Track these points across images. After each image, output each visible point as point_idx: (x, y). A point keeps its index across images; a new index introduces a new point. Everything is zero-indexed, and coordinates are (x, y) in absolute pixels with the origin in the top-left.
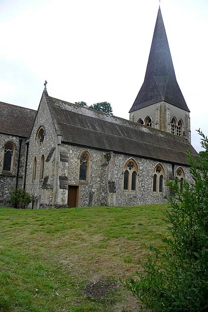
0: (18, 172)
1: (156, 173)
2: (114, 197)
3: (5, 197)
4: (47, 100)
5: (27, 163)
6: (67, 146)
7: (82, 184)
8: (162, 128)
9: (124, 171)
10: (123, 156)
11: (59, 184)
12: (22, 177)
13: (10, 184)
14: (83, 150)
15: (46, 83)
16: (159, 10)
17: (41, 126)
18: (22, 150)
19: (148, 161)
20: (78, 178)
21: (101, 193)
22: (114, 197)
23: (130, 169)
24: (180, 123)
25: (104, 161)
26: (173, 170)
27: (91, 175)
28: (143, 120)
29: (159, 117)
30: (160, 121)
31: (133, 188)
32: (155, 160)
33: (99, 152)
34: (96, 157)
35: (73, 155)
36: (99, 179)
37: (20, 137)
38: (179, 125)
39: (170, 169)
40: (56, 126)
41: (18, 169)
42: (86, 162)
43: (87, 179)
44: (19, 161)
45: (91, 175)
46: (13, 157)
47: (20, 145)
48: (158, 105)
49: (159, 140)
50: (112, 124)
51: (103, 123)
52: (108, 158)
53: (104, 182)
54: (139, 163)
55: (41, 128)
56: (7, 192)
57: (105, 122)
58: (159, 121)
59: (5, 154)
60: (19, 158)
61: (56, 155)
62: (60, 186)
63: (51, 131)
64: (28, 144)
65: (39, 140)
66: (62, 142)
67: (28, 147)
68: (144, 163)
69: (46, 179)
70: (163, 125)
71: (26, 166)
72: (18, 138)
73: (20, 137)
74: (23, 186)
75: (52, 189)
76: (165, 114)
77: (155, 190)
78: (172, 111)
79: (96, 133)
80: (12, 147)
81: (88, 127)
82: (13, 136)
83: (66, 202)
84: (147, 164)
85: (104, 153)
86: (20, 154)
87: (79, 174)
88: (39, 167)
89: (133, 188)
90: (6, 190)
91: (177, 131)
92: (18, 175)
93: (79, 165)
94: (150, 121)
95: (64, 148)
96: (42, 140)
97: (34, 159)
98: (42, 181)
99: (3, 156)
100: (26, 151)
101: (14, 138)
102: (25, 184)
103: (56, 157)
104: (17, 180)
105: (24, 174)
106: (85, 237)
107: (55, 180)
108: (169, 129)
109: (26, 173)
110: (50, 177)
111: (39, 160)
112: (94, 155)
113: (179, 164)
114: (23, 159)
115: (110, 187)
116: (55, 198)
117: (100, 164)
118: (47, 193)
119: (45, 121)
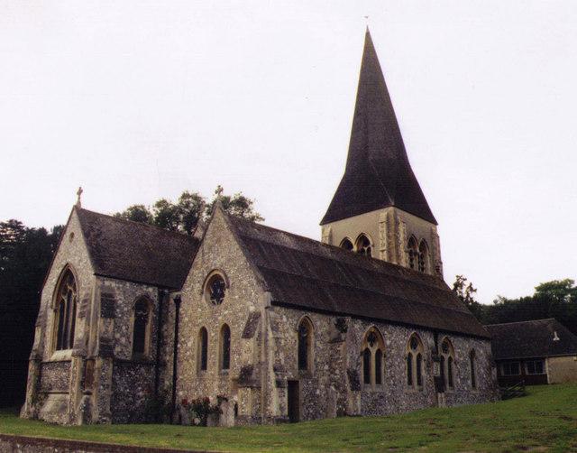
1: (411, 351)
2: (358, 397)
4: (81, 214)
8: (394, 258)
9: (364, 349)
10: (360, 322)
13: (145, 379)
14: (303, 315)
15: (80, 192)
16: (368, 34)
19: (398, 329)
20: (296, 366)
22: (358, 397)
23: (372, 346)
24: (423, 245)
25: (335, 332)
26: (436, 343)
27: (315, 360)
31: (378, 381)
32: (408, 326)
33: (326, 318)
34: (322, 325)
38: (421, 251)
39: (431, 341)
46: (148, 326)
53: (337, 372)
55: (215, 273)
56: (141, 393)
59: (136, 321)
64: (178, 301)
65: (209, 296)
70: (394, 252)
75: (259, 388)
76: (396, 230)
77: (410, 382)
78: (409, 221)
80: (147, 305)
82: (149, 285)
83: (286, 412)
84: (397, 336)
85: (334, 320)
87: (297, 359)
89: (378, 381)
97: (197, 329)
99: (133, 324)
101: (150, 289)
111: (214, 335)
112: (318, 323)
113: (445, 332)
114: (169, 329)
115: (113, 309)
116: (266, 405)
117: (328, 338)
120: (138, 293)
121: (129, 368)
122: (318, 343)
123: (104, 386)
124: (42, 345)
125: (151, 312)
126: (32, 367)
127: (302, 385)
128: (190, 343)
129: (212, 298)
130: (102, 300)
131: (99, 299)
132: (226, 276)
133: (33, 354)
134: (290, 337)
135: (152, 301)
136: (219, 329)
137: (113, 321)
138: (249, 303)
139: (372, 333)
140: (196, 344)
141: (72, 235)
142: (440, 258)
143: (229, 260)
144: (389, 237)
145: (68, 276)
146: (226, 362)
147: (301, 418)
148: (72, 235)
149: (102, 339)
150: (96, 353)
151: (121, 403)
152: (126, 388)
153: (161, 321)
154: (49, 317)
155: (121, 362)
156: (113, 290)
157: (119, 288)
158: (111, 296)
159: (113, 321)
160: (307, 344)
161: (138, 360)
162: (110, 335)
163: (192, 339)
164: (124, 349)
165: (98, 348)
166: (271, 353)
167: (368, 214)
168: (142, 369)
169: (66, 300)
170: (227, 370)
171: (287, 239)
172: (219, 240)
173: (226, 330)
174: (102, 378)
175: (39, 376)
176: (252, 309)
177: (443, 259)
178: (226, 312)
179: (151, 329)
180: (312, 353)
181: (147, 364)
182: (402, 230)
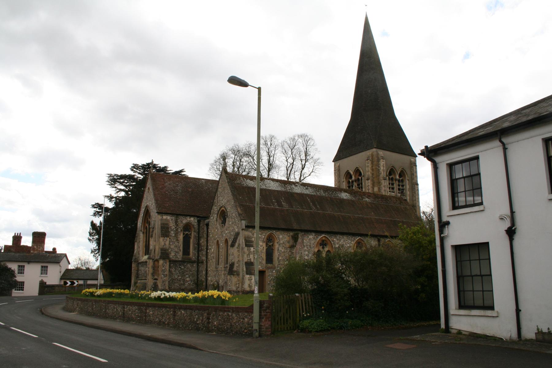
0: (198, 256)
3: (186, 285)
5: (207, 246)
6: (251, 229)
7: (269, 268)
9: (316, 250)
10: (314, 234)
11: (245, 269)
12: (202, 262)
13: (191, 271)
14: (268, 233)
18: (201, 231)
19: (345, 237)
20: (264, 262)
23: (323, 248)
27: (278, 258)
28: (352, 173)
29: (370, 171)
30: (373, 174)
32: (354, 235)
38: (400, 176)
40: (239, 209)
41: (198, 254)
42: (272, 245)
43: (274, 263)
44: (199, 244)
45: (278, 258)
46: (192, 241)
48: (368, 153)
50: (301, 195)
52: (295, 239)
54: (333, 241)
56: (188, 279)
58: (370, 175)
59: (184, 238)
60: (199, 241)
61: (241, 240)
62: (246, 272)
63: (234, 215)
64: (207, 225)
65: (221, 222)
66: (246, 227)
67: (208, 229)
68: (340, 240)
69: (232, 265)
71: (207, 249)
72: (196, 218)
73: (198, 217)
74: (204, 273)
76: (378, 165)
78: (388, 158)
80: (190, 229)
81: (273, 205)
82: (191, 216)
84: (344, 241)
85: (291, 234)
86: (199, 236)
87: (264, 257)
88: (222, 251)
91: (399, 185)
93: (265, 248)
94: (360, 174)
95: (247, 233)
96: (224, 222)
97: (215, 242)
98: (227, 267)
100: (206, 232)
101: (192, 219)
102: (207, 270)
103: (241, 243)
104: (198, 266)
105: (204, 258)
107: (241, 266)
108: (385, 189)
109: (207, 258)
110: (235, 263)
112: (281, 237)
114: (203, 241)
117: (288, 245)
118: (234, 279)
119: (225, 199)
120: (184, 222)
121: (180, 265)
122: (280, 249)
125: (193, 233)
127: (268, 273)
130: (161, 227)
131: (160, 226)
134: (262, 246)
136: (224, 241)
137: (168, 239)
138: (235, 227)
139: (323, 241)
142: (417, 181)
143: (228, 201)
144: (373, 170)
145: (147, 213)
149: (162, 249)
151: (176, 284)
153: (199, 238)
154: (141, 237)
155: (175, 262)
156: (168, 221)
158: (167, 224)
159: (168, 239)
160: (273, 249)
162: (167, 246)
164: (176, 253)
166: (245, 256)
167: (361, 154)
171: (512, 118)
173: (226, 241)
174: (163, 271)
176: (237, 230)
177: (419, 181)
179: (193, 241)
180: (276, 254)
182: (382, 164)
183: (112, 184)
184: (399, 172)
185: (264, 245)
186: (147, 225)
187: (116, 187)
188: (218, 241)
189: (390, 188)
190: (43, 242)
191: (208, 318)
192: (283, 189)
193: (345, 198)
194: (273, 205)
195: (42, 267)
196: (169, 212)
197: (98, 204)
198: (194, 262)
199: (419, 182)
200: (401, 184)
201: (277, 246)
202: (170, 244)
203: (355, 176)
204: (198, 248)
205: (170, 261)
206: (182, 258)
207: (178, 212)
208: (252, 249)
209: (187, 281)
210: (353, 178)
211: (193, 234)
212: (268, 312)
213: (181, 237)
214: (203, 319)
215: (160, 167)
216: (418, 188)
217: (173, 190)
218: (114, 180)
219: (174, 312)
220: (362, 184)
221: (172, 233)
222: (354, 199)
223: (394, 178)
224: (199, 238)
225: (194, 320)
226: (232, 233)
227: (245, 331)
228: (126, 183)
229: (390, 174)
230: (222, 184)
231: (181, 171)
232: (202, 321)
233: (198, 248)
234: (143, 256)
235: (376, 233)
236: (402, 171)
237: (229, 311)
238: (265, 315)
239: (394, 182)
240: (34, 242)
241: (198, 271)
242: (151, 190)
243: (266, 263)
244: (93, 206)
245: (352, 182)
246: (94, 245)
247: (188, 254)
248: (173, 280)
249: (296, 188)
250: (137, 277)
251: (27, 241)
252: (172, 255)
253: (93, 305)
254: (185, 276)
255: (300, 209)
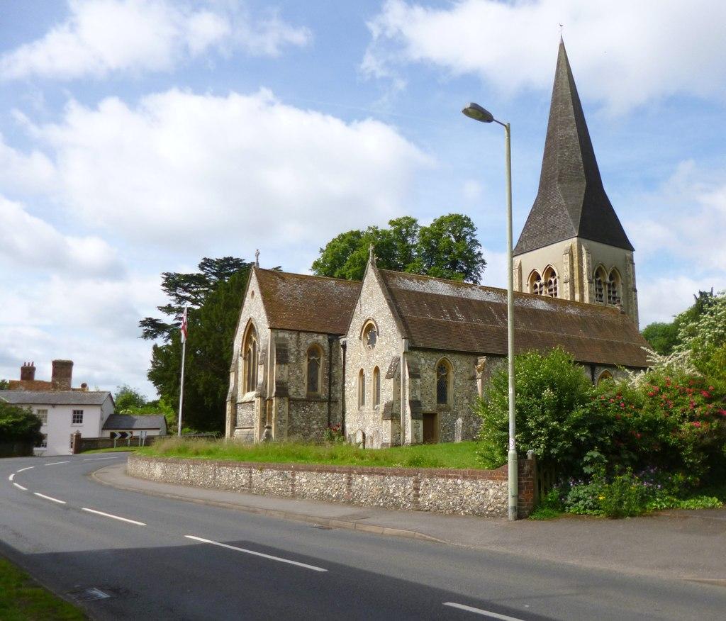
0: (330, 392)
6: (416, 353)
12: (336, 402)
13: (319, 414)
14: (441, 357)
16: (562, 46)
17: (368, 320)
20: (435, 401)
21: (471, 423)
27: (455, 396)
33: (465, 358)
35: (426, 367)
36: (466, 401)
37: (329, 334)
38: (611, 278)
42: (446, 376)
43: (448, 402)
44: (330, 375)
45: (455, 396)
46: (320, 369)
47: (331, 347)
49: (570, 322)
50: (481, 303)
51: (466, 305)
56: (315, 427)
57: (469, 302)
59: (309, 365)
63: (389, 330)
64: (344, 347)
65: (366, 342)
71: (344, 383)
79: (458, 326)
81: (445, 317)
82: (319, 333)
86: (330, 363)
87: (436, 395)
90: (314, 425)
91: (609, 292)
92: (330, 398)
93: (436, 380)
94: (553, 274)
97: (358, 371)
99: (306, 368)
101: (321, 337)
106: (73, 597)
111: (369, 375)
112: (458, 363)
120: (310, 341)
123: (281, 421)
124: (236, 388)
125: (322, 357)
126: (229, 407)
128: (352, 383)
129: (368, 344)
132: (377, 325)
133: (229, 396)
134: (430, 377)
135: (322, 347)
136: (373, 371)
137: (287, 367)
138: (393, 349)
140: (358, 383)
141: (253, 293)
143: (379, 311)
145: (251, 329)
146: (377, 401)
147: (187, 429)
148: (253, 293)
150: (273, 395)
152: (302, 422)
153: (331, 366)
154: (240, 364)
156: (287, 340)
157: (291, 338)
158: (284, 345)
159: (287, 367)
161: (312, 398)
162: (285, 378)
163: (354, 378)
165: (275, 390)
168: (316, 406)
169: (252, 350)
170: (379, 406)
172: (371, 294)
173: (377, 370)
175: (235, 414)
178: (377, 356)
179: (323, 371)
180: (451, 390)
181: (319, 400)
183: (171, 290)
184: (609, 273)
185: (435, 375)
186: (251, 347)
187: (177, 295)
188: (362, 370)
189: (597, 295)
190: (69, 375)
191: (417, 489)
192: (456, 295)
193: (541, 308)
194: (445, 317)
195: (75, 412)
196: (286, 327)
197: (150, 319)
198: (322, 401)
199: (638, 288)
200: (611, 289)
201: (452, 376)
202: (289, 375)
203: (546, 278)
204: (330, 380)
205: (289, 400)
206: (307, 396)
207: (300, 328)
208: (419, 381)
209: (315, 430)
210: (543, 281)
211: (323, 360)
212: (531, 479)
213: (305, 364)
214: (405, 489)
215: (245, 264)
216: (636, 295)
217: (291, 295)
218: (173, 283)
219: (350, 479)
220: (556, 289)
221: (292, 358)
222: (553, 310)
223: (603, 281)
224: (331, 366)
225: (388, 492)
226: (387, 358)
227: (490, 509)
228: (193, 288)
229: (597, 275)
230: (368, 286)
231: (280, 267)
232: (404, 493)
233: (330, 380)
234: (244, 394)
235: (588, 359)
236: (613, 272)
237: (458, 478)
238: (527, 484)
239: (603, 286)
240: (54, 374)
241: (329, 414)
242: (258, 294)
243: (438, 403)
244: (144, 323)
245: (541, 286)
246: (658, 323)
247: (316, 389)
248: (293, 428)
249: (474, 292)
250: (234, 424)
251: (44, 373)
252: (292, 391)
253: (189, 469)
254: (310, 421)
255: (481, 324)
